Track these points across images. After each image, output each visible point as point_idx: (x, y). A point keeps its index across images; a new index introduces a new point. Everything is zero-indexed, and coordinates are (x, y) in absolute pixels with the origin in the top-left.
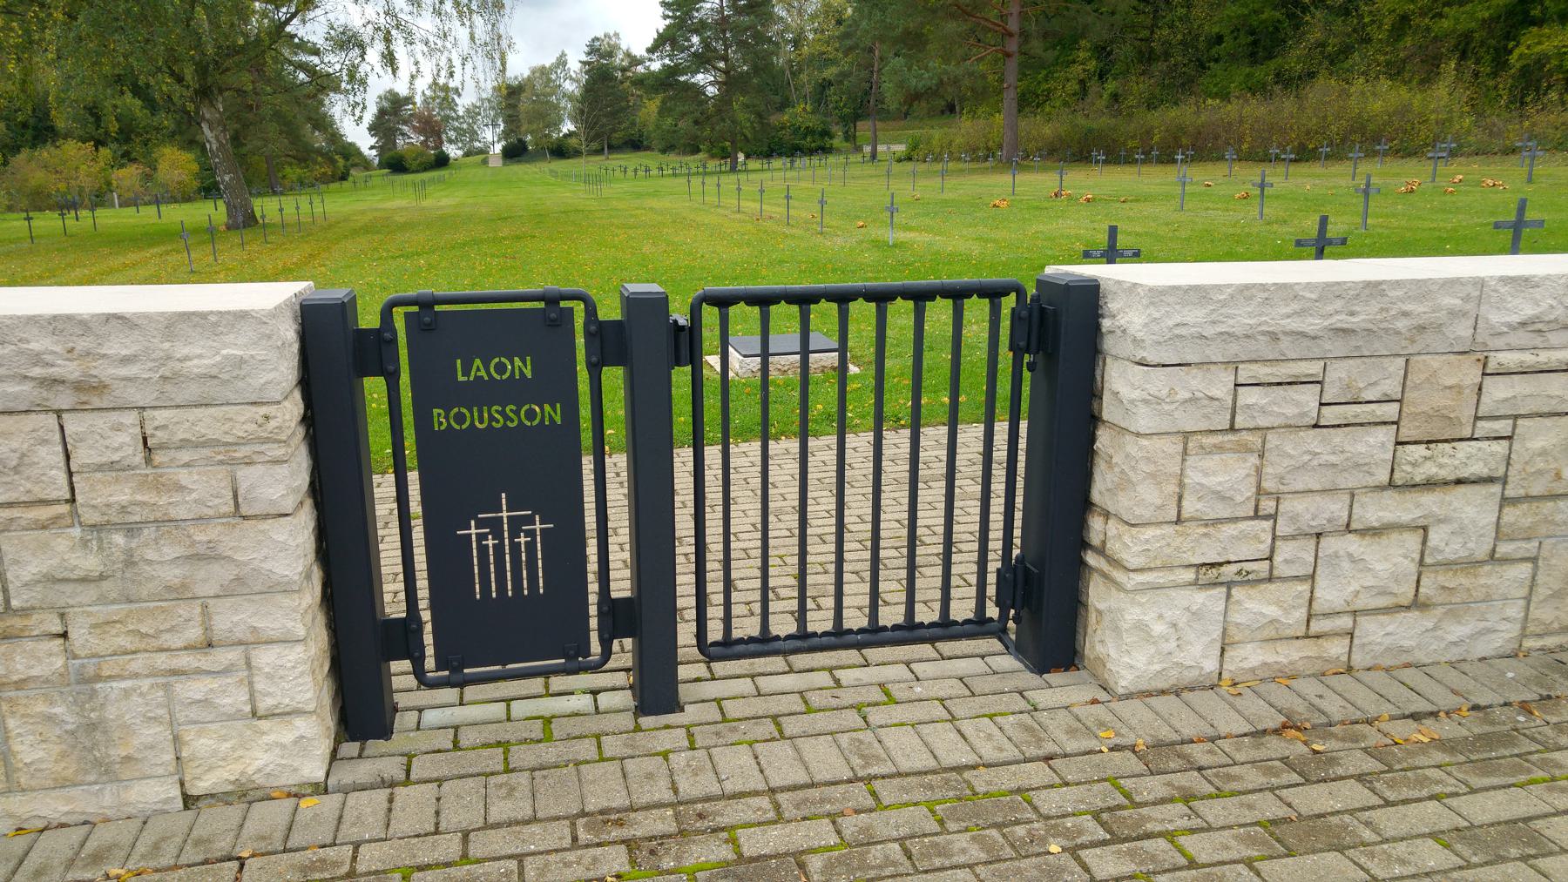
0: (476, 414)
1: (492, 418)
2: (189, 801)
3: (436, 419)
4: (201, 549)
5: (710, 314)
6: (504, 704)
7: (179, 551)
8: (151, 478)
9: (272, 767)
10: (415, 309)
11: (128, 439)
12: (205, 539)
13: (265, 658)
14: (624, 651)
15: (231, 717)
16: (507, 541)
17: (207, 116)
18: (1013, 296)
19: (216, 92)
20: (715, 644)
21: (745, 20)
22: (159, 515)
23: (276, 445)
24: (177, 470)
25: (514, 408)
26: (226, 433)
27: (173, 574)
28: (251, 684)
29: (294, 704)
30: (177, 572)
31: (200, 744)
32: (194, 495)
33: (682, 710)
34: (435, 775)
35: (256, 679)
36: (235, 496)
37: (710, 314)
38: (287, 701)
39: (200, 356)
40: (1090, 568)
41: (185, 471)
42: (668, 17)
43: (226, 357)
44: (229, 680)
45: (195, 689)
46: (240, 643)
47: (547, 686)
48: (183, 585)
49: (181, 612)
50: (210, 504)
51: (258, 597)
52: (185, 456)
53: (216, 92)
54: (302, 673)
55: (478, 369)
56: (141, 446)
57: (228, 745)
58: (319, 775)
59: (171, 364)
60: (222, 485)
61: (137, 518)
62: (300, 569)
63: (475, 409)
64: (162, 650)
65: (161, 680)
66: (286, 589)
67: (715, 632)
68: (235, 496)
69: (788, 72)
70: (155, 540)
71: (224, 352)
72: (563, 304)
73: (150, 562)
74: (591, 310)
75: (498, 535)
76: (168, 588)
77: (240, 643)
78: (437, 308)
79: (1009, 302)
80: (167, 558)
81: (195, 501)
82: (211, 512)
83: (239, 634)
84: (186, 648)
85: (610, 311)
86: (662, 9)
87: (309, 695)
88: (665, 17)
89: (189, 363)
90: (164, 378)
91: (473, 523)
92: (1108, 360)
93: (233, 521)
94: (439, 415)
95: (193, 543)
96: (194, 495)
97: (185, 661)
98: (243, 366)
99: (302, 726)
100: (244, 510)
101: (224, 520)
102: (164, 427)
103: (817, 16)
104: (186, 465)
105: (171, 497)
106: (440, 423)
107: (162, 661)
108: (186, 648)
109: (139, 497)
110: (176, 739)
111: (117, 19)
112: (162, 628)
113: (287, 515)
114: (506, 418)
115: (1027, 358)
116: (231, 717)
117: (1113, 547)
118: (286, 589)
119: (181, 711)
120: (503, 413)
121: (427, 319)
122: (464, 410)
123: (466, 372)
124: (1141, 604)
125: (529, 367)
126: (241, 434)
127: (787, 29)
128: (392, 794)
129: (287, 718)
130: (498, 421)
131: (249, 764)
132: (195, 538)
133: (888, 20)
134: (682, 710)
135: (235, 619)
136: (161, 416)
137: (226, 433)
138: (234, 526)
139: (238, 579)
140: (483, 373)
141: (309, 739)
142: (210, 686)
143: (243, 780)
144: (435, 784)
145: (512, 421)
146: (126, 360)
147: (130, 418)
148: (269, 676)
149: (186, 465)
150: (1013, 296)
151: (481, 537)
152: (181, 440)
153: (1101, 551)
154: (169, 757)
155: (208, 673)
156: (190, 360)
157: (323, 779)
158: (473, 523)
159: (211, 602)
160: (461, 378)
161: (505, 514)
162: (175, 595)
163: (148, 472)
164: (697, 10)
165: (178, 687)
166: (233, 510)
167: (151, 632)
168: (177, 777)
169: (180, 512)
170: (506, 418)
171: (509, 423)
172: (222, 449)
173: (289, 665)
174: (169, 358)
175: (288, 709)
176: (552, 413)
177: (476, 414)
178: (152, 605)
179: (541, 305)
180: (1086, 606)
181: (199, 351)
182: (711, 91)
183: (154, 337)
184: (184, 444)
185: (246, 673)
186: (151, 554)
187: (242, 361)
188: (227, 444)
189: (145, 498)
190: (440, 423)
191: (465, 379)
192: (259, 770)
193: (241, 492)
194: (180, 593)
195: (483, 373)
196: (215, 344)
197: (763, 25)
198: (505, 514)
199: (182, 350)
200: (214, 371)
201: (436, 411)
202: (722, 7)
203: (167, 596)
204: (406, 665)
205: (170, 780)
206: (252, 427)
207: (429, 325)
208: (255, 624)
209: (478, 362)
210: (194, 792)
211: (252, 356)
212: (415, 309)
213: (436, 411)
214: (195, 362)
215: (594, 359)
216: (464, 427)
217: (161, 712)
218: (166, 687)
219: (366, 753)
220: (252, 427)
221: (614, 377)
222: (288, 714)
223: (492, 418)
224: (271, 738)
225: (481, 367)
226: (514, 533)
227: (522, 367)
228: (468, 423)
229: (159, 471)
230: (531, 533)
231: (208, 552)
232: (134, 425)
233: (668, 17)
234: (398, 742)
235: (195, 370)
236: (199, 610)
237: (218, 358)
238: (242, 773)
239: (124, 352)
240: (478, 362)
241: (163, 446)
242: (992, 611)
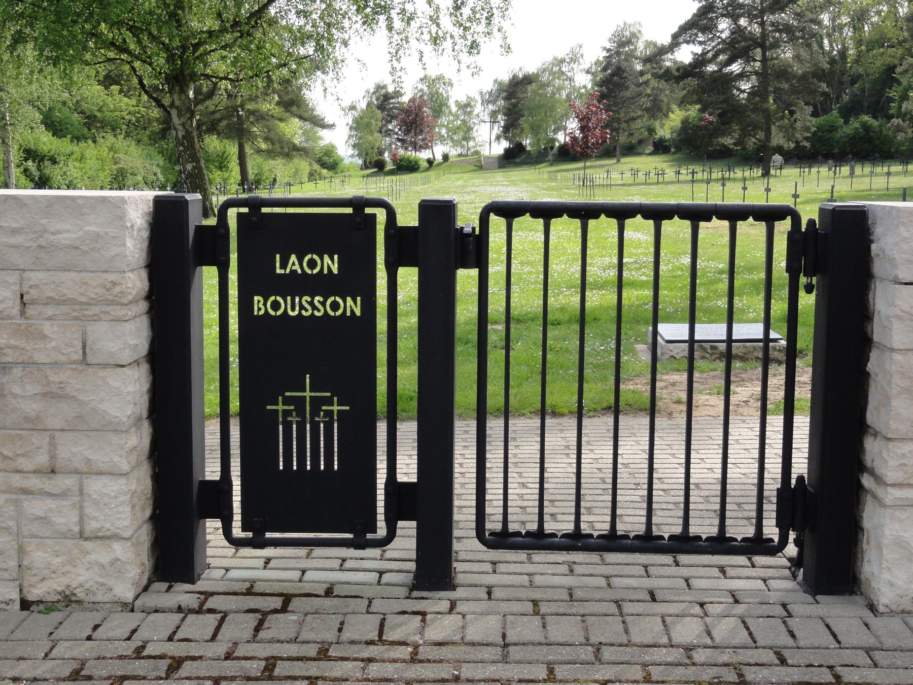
0: (289, 302)
1: (302, 307)
2: (25, 605)
4: (54, 388)
5: (497, 223)
7: (38, 389)
8: (22, 328)
9: (91, 583)
10: (245, 210)
11: (9, 295)
12: (57, 380)
13: (95, 486)
14: (407, 529)
15: (65, 536)
18: (788, 220)
22: (26, 357)
23: (119, 307)
24: (42, 322)
25: (321, 299)
26: (82, 294)
27: (31, 407)
28: (81, 508)
29: (113, 529)
30: (35, 406)
31: (38, 557)
32: (53, 344)
35: (86, 504)
36: (84, 347)
37: (497, 223)
38: (108, 525)
39: (68, 231)
40: (867, 491)
41: (48, 323)
43: (87, 233)
44: (65, 503)
45: (37, 507)
46: (77, 472)
48: (38, 418)
49: (34, 440)
50: (64, 351)
51: (93, 434)
52: (50, 311)
54: (122, 503)
55: (293, 264)
56: (18, 301)
57: (59, 560)
58: (129, 596)
59: (47, 236)
60: (75, 336)
61: (9, 359)
62: (129, 413)
63: (289, 298)
64: (18, 471)
65: (14, 497)
66: (115, 428)
67: (493, 524)
68: (84, 347)
70: (21, 378)
71: (86, 228)
72: (368, 210)
73: (15, 396)
74: (391, 215)
75: (301, 411)
76: (27, 419)
77: (77, 472)
78: (265, 210)
79: (783, 227)
80: (28, 394)
81: (54, 348)
82: (63, 358)
83: (78, 464)
84: (35, 472)
85: (408, 218)
87: (127, 523)
89: (60, 236)
90: (40, 247)
91: (280, 398)
92: (877, 283)
93: (80, 367)
94: (259, 302)
95: (48, 383)
96: (53, 344)
97: (34, 482)
98: (100, 240)
99: (120, 550)
100: (90, 359)
101: (74, 366)
102: (36, 286)
104: (50, 318)
105: (36, 344)
106: (259, 309)
107: (17, 480)
108: (35, 472)
109: (13, 342)
110: (21, 551)
112: (19, 452)
113: (122, 366)
114: (314, 308)
115: (803, 280)
116: (65, 536)
117: (880, 470)
118: (115, 428)
119: (26, 525)
120: (311, 303)
123: (284, 265)
124: (901, 521)
125: (336, 265)
126: (92, 296)
129: (107, 542)
130: (306, 310)
131: (74, 579)
132: (51, 379)
135: (74, 450)
136: (36, 277)
137: (82, 294)
138: (80, 372)
139: (80, 417)
140: (297, 267)
141: (122, 562)
142: (50, 506)
143: (67, 593)
145: (319, 310)
146: (15, 232)
147: (13, 278)
148: (96, 503)
149: (50, 318)
150: (788, 220)
152: (48, 298)
153: (872, 473)
154: (13, 564)
155: (50, 495)
156: (61, 234)
157: (131, 601)
158: (280, 398)
159: (57, 434)
160: (278, 271)
161: (308, 394)
162: (30, 426)
163: (22, 322)
165: (26, 504)
166: (81, 358)
167: (10, 454)
168: (17, 583)
169: (41, 357)
170: (314, 308)
172: (77, 307)
173: (113, 494)
174: (45, 231)
175: (108, 533)
176: (353, 306)
177: (289, 302)
178: (13, 432)
179: (349, 210)
180: (863, 530)
181: (68, 227)
183: (36, 214)
184: (50, 301)
185: (78, 498)
186: (17, 390)
187: (98, 235)
188: (81, 303)
189: (17, 343)
191: (283, 272)
192: (81, 586)
193: (89, 343)
194: (34, 424)
195: (297, 267)
196: (79, 222)
198: (308, 394)
199: (54, 226)
200: (77, 243)
201: (256, 298)
203: (25, 426)
204: (218, 523)
205: (12, 584)
206: (101, 291)
208: (90, 457)
209: (293, 258)
210: (30, 598)
211: (107, 233)
212: (245, 210)
213: (256, 298)
214: (65, 235)
217: (11, 523)
218: (17, 503)
220: (101, 291)
221: (408, 277)
222: (108, 538)
223: (302, 307)
224: (92, 557)
225: (297, 263)
226: (315, 412)
227: (331, 264)
229: (30, 321)
231: (59, 391)
232: (15, 284)
234: (201, 586)
235: (64, 242)
236: (47, 440)
237: (80, 233)
238: (68, 586)
239: (15, 225)
240: (293, 258)
241: (34, 302)
242: (771, 531)
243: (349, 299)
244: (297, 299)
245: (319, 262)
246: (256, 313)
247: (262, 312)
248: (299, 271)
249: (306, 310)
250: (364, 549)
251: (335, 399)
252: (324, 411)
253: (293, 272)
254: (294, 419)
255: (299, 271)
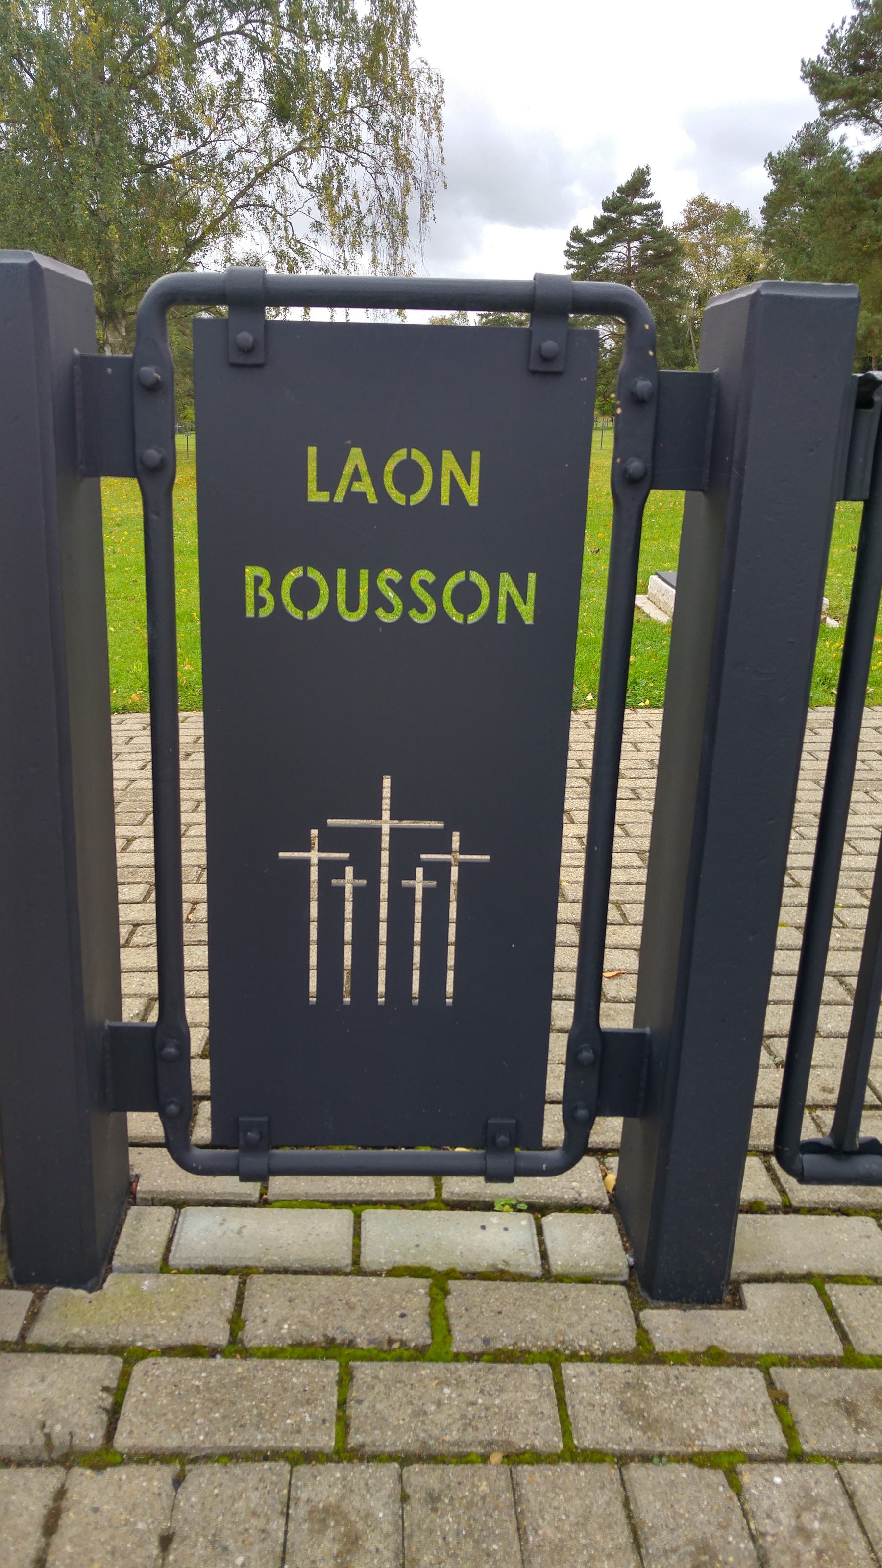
1: (377, 599)
3: (250, 592)
6: (347, 1214)
16: (384, 889)
17: (111, 339)
19: (120, 316)
20: (814, 1147)
21: (651, 271)
25: (430, 577)
33: (738, 1304)
34: (172, 1442)
42: (572, 266)
47: (439, 1189)
53: (120, 316)
55: (356, 476)
63: (342, 574)
69: (690, 329)
78: (271, 314)
86: (567, 259)
88: (569, 266)
91: (314, 832)
94: (258, 581)
103: (727, 272)
106: (260, 602)
111: (30, 235)
114: (411, 601)
120: (402, 589)
121: (246, 337)
122: (314, 574)
123: (328, 482)
127: (693, 284)
128: (61, 1493)
130: (389, 608)
133: (815, 267)
134: (738, 1304)
140: (365, 486)
144: (168, 1472)
145: (422, 609)
151: (330, 869)
161: (314, 856)
164: (603, 260)
171: (414, 614)
182: (609, 344)
190: (260, 602)
191: (323, 497)
195: (365, 486)
197: (670, 277)
198: (314, 856)
201: (251, 572)
202: (629, 257)
207: (249, 351)
209: (356, 458)
213: (251, 572)
215: (636, 466)
216: (312, 615)
219: (41, 1333)
223: (377, 599)
225: (363, 468)
228: (322, 605)
230: (437, 872)
233: (572, 266)
240: (356, 458)
243: (505, 579)
244: (364, 574)
245: (485, 590)
246: (250, 613)
247: (265, 612)
248: (372, 499)
249: (389, 608)
250: (510, 1180)
251: (456, 837)
252: (426, 865)
253: (355, 499)
254: (349, 881)
255: (372, 499)
